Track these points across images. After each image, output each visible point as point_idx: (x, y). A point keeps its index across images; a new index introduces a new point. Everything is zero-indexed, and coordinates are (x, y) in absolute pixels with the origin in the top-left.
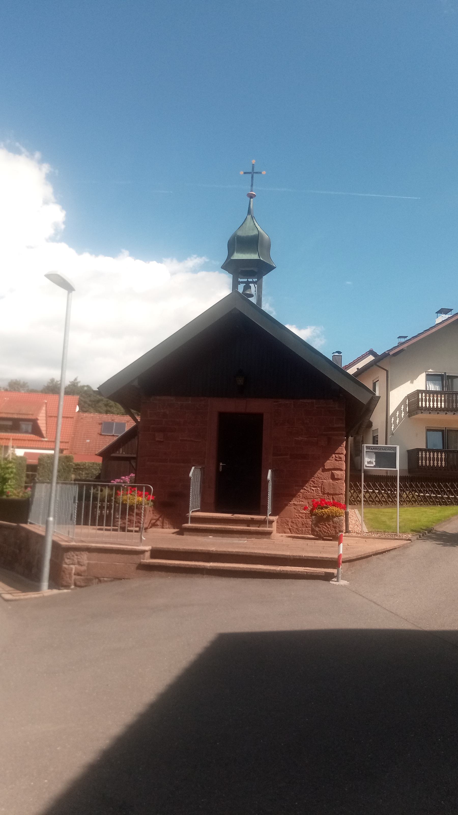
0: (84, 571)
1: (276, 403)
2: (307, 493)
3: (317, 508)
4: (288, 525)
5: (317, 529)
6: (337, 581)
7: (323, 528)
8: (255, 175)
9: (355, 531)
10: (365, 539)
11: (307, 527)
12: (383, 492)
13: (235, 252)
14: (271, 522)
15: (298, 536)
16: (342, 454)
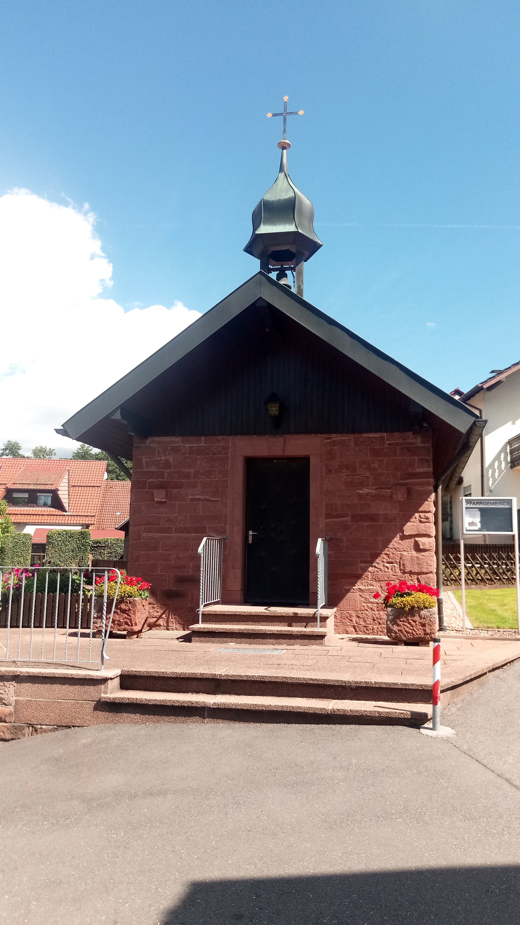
0: (10, 714)
1: (328, 441)
2: (379, 571)
3: (395, 596)
4: (351, 621)
5: (395, 628)
6: (433, 729)
7: (404, 626)
8: (288, 117)
9: (454, 627)
10: (470, 641)
11: (380, 624)
12: (486, 566)
13: (262, 224)
14: (324, 619)
15: (367, 639)
16: (429, 512)
